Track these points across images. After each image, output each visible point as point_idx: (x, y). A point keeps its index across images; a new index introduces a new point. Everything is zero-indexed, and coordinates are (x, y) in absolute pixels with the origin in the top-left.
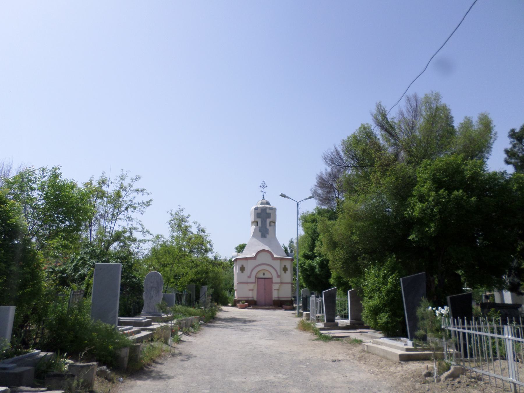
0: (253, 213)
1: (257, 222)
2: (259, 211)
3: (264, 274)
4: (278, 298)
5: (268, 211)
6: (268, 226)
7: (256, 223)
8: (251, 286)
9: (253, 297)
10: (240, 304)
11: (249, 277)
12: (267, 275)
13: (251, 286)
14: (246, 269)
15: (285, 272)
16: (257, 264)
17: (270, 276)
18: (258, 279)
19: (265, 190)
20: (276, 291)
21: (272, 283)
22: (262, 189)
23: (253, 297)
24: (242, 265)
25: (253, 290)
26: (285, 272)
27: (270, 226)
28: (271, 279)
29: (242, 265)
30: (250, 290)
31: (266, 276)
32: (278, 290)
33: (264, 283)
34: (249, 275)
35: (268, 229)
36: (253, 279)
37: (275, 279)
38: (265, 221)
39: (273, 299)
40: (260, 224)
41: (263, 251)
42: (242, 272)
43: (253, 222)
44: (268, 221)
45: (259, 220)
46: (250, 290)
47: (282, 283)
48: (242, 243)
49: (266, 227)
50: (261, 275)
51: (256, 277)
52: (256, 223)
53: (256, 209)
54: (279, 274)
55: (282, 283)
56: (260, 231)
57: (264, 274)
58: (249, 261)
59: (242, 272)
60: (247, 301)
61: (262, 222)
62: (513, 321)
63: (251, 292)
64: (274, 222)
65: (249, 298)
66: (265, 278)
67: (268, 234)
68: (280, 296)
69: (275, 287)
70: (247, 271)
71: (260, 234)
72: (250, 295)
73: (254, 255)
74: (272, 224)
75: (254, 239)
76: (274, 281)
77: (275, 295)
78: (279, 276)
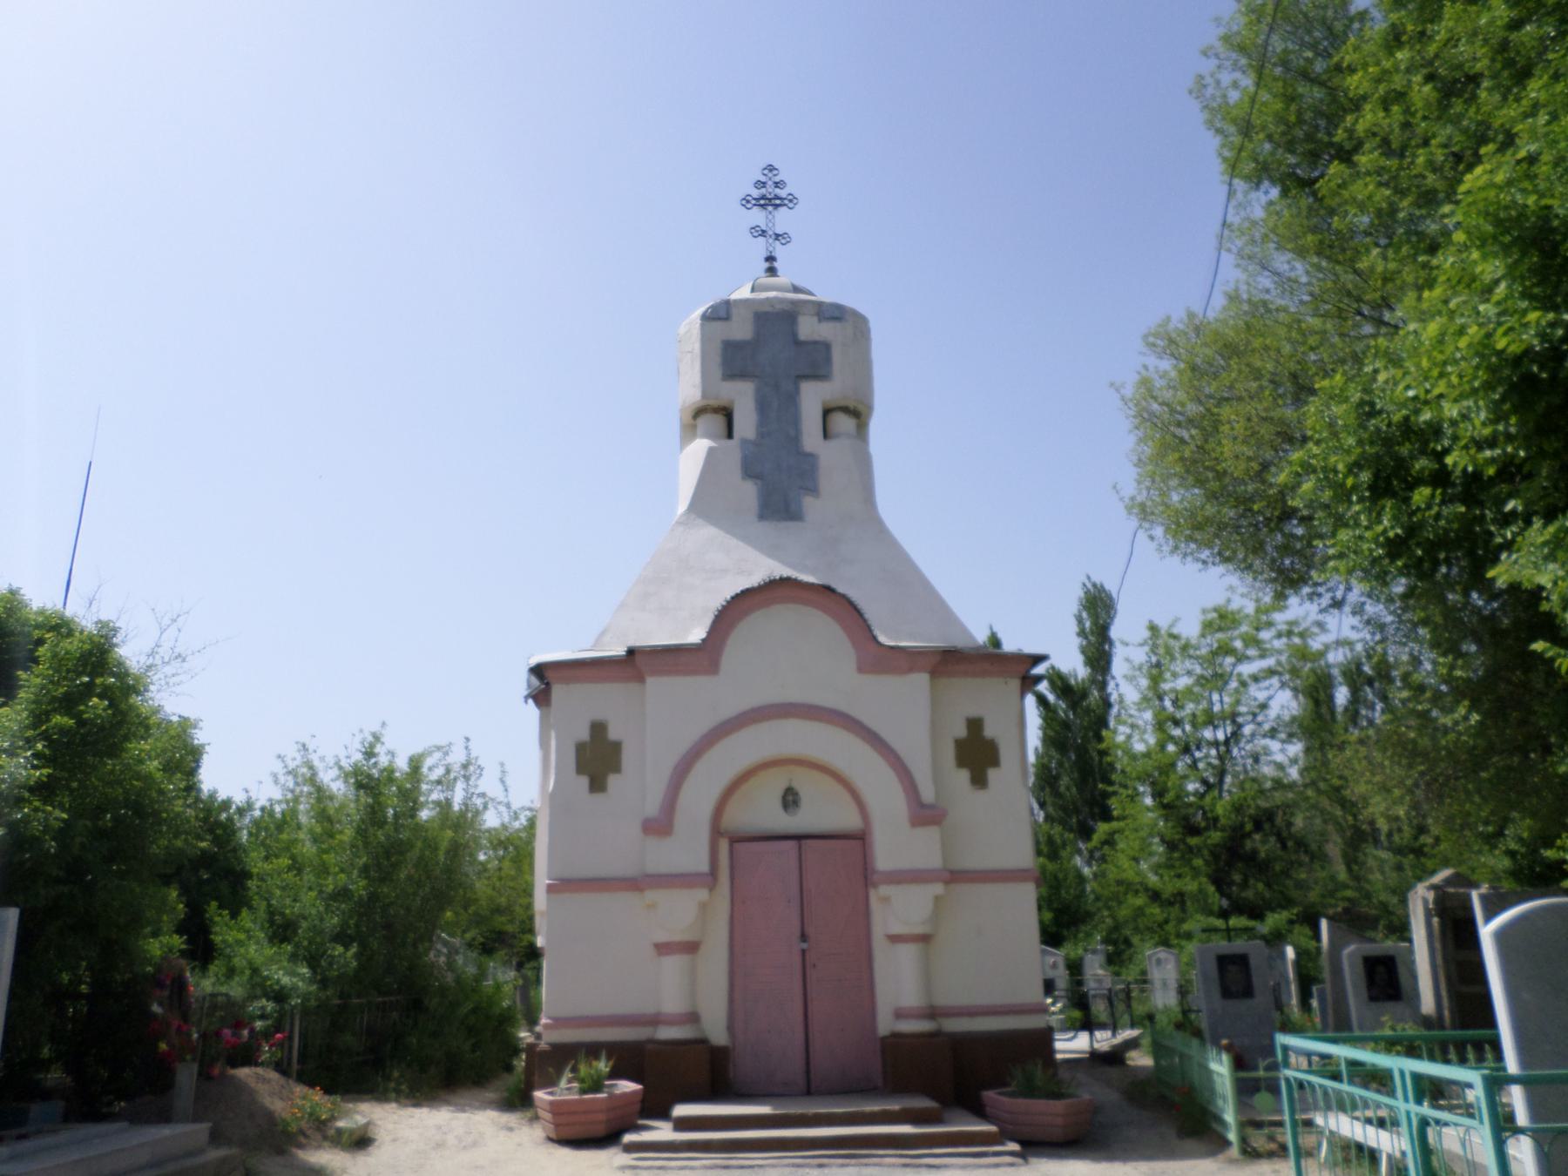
0: (696, 346)
1: (727, 414)
2: (741, 330)
3: (790, 800)
4: (932, 1013)
5: (808, 328)
6: (811, 437)
7: (715, 414)
8: (677, 913)
9: (693, 1018)
10: (565, 1090)
11: (659, 826)
12: (824, 811)
13: (677, 913)
14: (628, 758)
15: (979, 781)
16: (731, 707)
17: (843, 818)
18: (734, 843)
19: (783, 220)
20: (907, 955)
21: (867, 875)
22: (758, 217)
23: (693, 1018)
24: (598, 729)
25: (691, 948)
26: (979, 781)
27: (826, 434)
28: (860, 838)
29: (598, 729)
30: (663, 949)
31: (807, 819)
32: (924, 939)
33: (798, 878)
34: (652, 807)
35: (811, 459)
36: (688, 849)
37: (897, 844)
38: (791, 401)
39: (886, 1024)
40: (746, 423)
41: (775, 590)
42: (597, 785)
43: (699, 412)
44: (812, 397)
45: (742, 397)
46: (663, 949)
47: (955, 877)
48: (779, 793)
49: (795, 439)
50: (761, 810)
51: (717, 832)
52: (718, 421)
53: (719, 314)
54: (928, 794)
55: (955, 877)
56: (750, 470)
57: (790, 800)
58: (658, 687)
59: (597, 785)
60: (628, 1059)
61: (762, 407)
62: (448, 852)
63: (673, 965)
64: (858, 414)
65: (655, 1020)
66: (799, 837)
67: (814, 491)
68: (948, 996)
69: (898, 910)
70: (640, 781)
71: (749, 492)
72: (672, 1003)
73: (696, 635)
74: (842, 422)
75: (707, 532)
76: (885, 857)
77: (900, 991)
78: (925, 815)
